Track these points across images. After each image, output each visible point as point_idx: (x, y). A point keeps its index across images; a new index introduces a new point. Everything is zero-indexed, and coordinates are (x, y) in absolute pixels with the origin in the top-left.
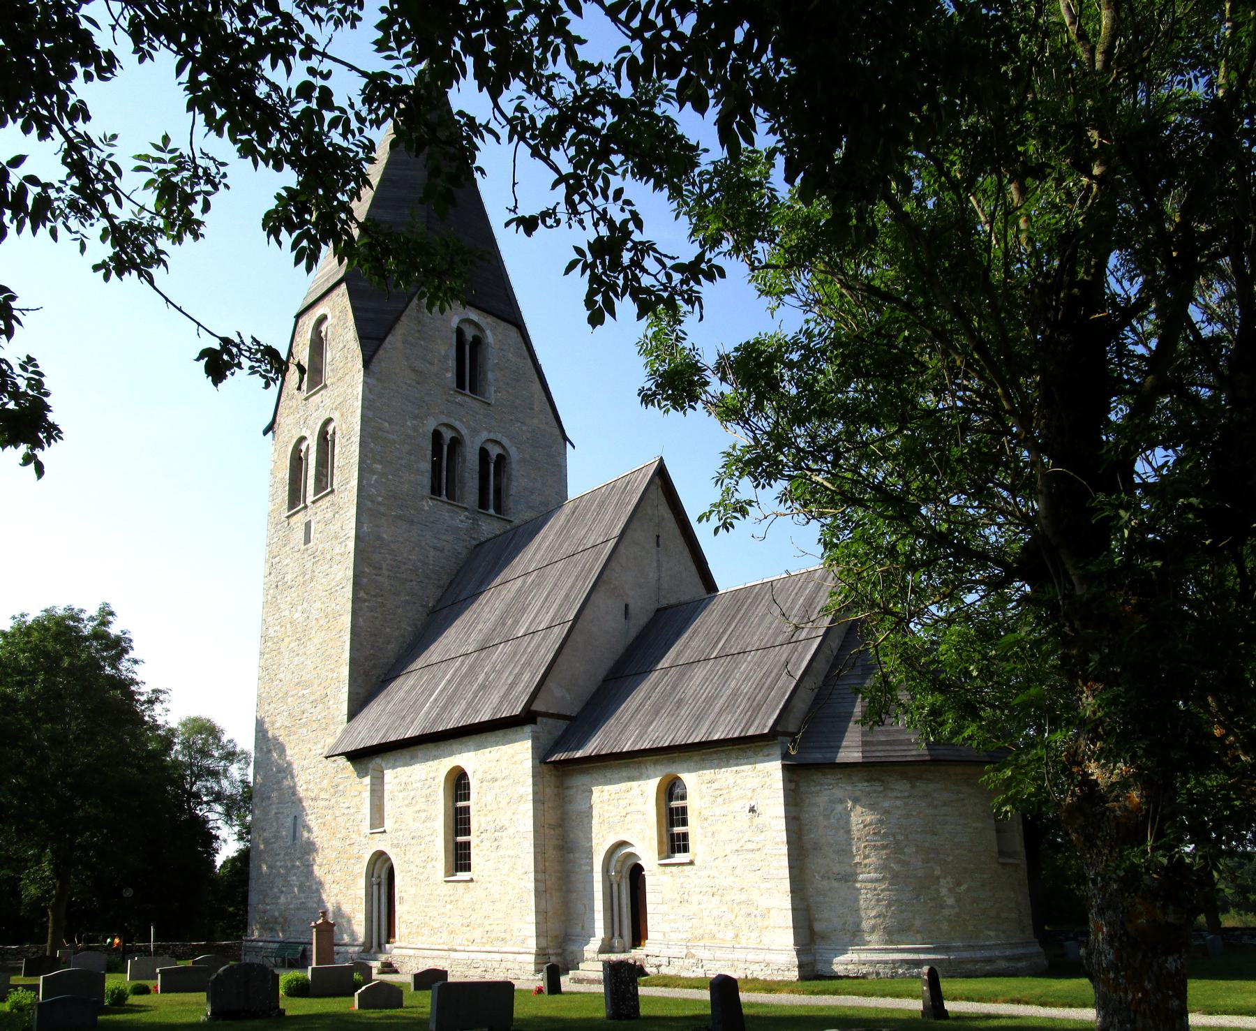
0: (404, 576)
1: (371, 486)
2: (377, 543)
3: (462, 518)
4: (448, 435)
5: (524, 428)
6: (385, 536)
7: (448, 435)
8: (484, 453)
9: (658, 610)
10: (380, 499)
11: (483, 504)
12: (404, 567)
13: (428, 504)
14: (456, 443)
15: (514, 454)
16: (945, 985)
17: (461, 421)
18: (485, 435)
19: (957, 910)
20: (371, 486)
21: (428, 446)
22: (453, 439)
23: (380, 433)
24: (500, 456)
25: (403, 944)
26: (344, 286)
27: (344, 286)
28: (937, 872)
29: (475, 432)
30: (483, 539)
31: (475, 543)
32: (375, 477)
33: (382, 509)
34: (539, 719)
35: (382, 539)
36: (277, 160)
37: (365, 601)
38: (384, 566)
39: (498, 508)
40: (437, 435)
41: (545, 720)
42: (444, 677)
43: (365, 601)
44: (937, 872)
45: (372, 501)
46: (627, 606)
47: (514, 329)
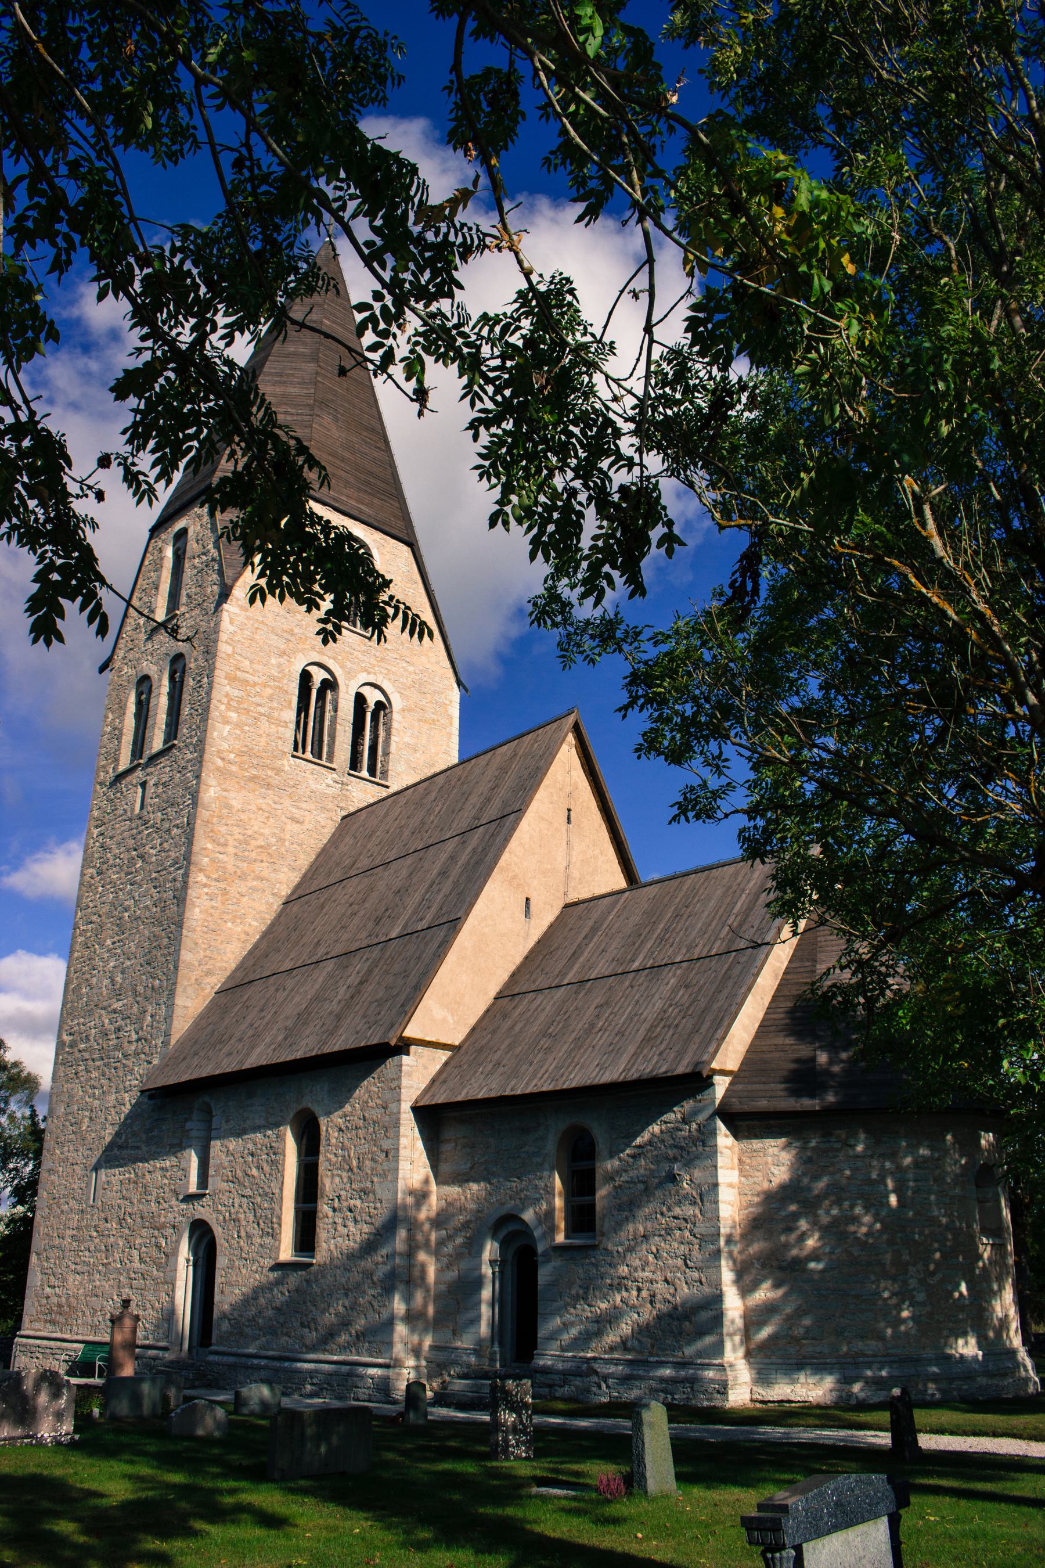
0: (253, 855)
1: (224, 739)
2: (225, 811)
3: (330, 781)
4: (319, 676)
5: (411, 669)
6: (234, 803)
7: (319, 676)
8: (360, 700)
9: (567, 906)
10: (232, 756)
11: (355, 764)
12: (253, 843)
13: (289, 763)
14: (330, 685)
15: (397, 703)
16: (920, 1416)
17: (334, 658)
18: (364, 678)
19: (929, 1308)
20: (224, 739)
21: (294, 688)
22: (325, 682)
23: (239, 673)
24: (379, 705)
25: (221, 1348)
26: (444, 1056)
27: (444, 1056)
28: (906, 1257)
29: (350, 674)
30: (352, 809)
31: (345, 813)
32: (228, 728)
33: (234, 768)
34: (413, 1048)
35: (229, 807)
36: (78, 204)
37: (205, 885)
38: (231, 842)
39: (372, 771)
40: (306, 677)
41: (420, 1049)
42: (314, 67)
43: (205, 885)
44: (906, 1257)
45: (223, 759)
46: (528, 899)
47: (405, 550)
